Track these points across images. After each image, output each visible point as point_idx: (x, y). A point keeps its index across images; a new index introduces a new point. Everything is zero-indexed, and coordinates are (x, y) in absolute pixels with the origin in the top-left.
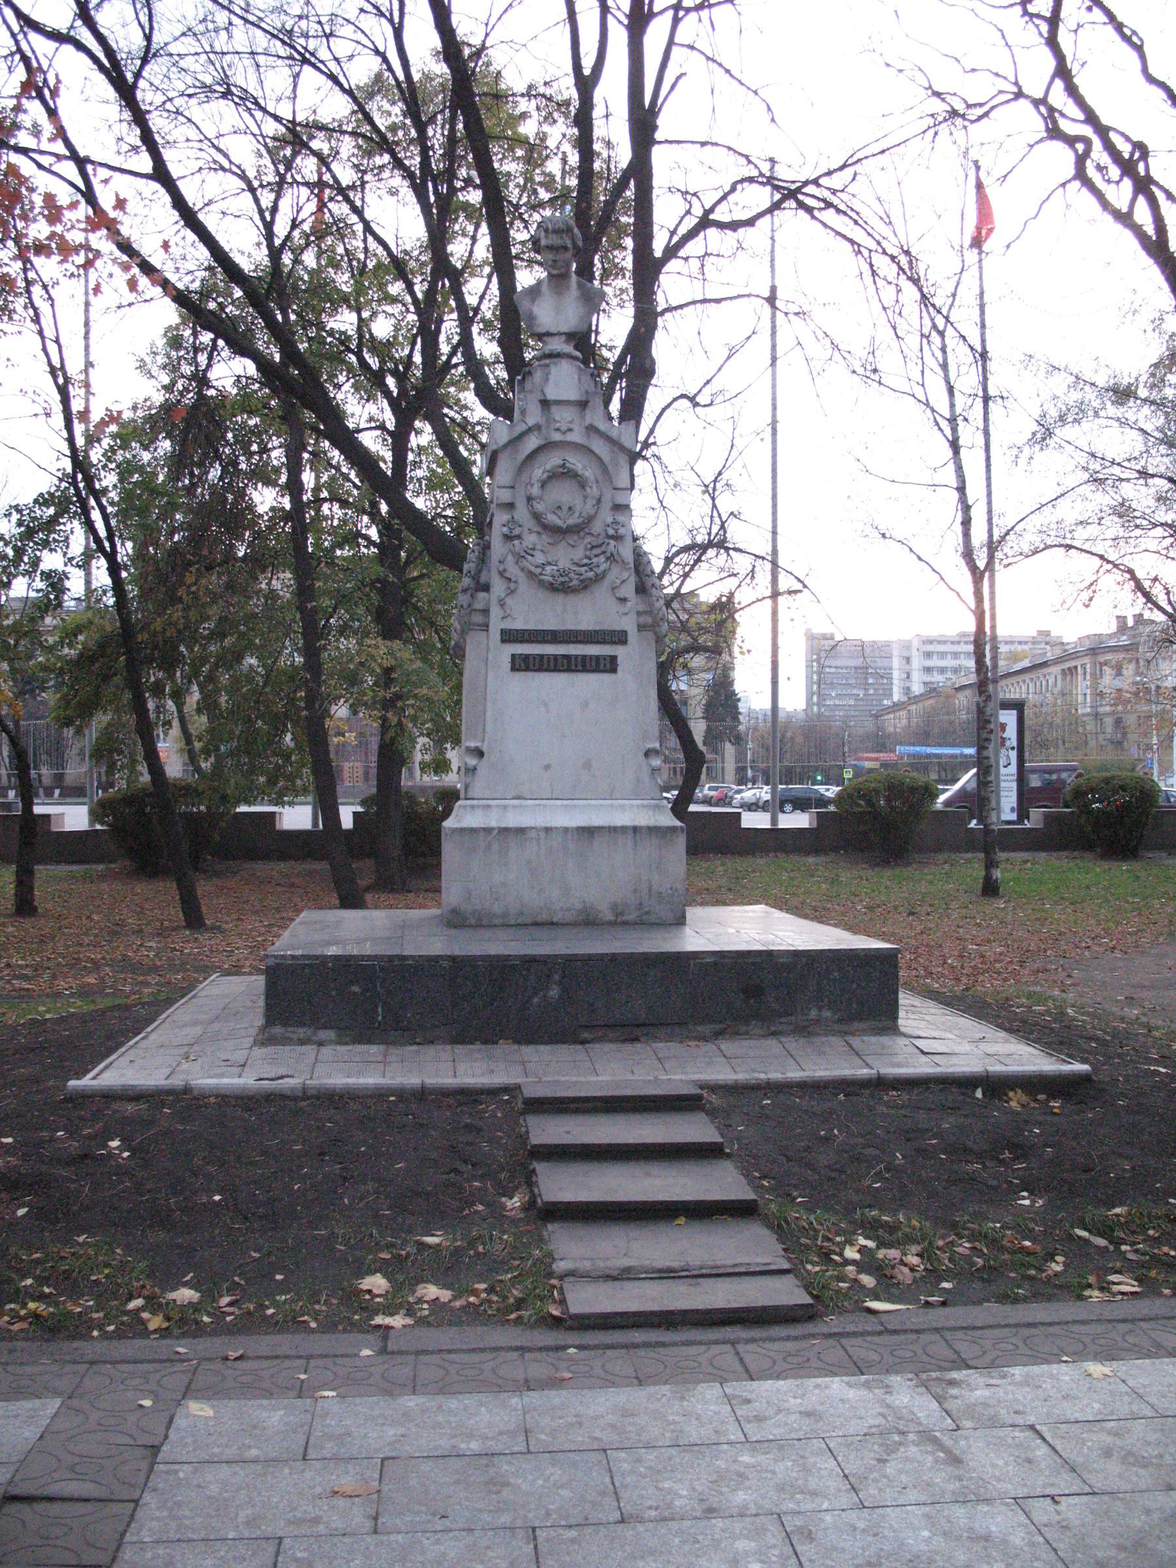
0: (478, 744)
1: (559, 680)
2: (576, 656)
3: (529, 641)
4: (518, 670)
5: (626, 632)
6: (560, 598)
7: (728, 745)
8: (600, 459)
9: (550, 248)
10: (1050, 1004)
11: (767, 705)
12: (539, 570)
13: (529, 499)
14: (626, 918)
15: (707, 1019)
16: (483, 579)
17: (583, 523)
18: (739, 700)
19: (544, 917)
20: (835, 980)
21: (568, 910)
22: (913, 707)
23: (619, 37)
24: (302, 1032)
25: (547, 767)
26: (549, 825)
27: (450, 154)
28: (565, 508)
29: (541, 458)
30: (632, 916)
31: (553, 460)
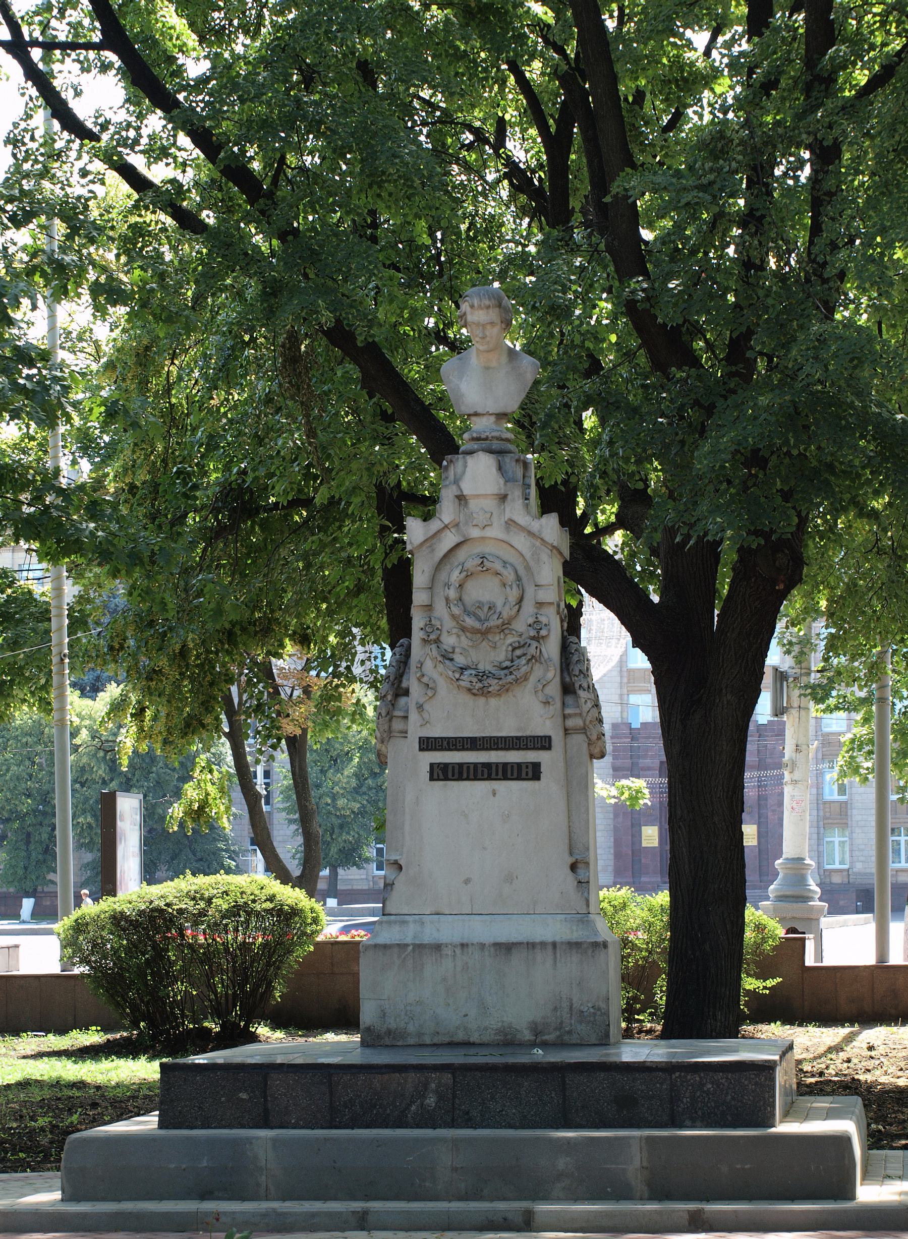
0: (397, 858)
1: (478, 789)
2: (497, 764)
3: (441, 748)
4: (438, 779)
5: (550, 737)
6: (482, 700)
19: (461, 1036)
21: (486, 1029)
25: (467, 881)
28: (486, 609)
30: (550, 1037)
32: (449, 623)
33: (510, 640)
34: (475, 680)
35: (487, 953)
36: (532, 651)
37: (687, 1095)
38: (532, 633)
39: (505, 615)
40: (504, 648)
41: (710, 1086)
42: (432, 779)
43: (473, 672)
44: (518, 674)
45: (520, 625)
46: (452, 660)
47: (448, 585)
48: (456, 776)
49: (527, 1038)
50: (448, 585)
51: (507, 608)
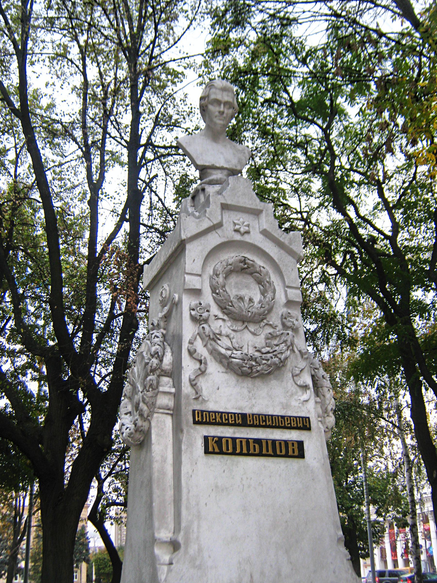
2: (267, 441)
4: (214, 453)
10: (331, 76)
12: (229, 353)
33: (269, 330)
42: (207, 452)
48: (230, 451)
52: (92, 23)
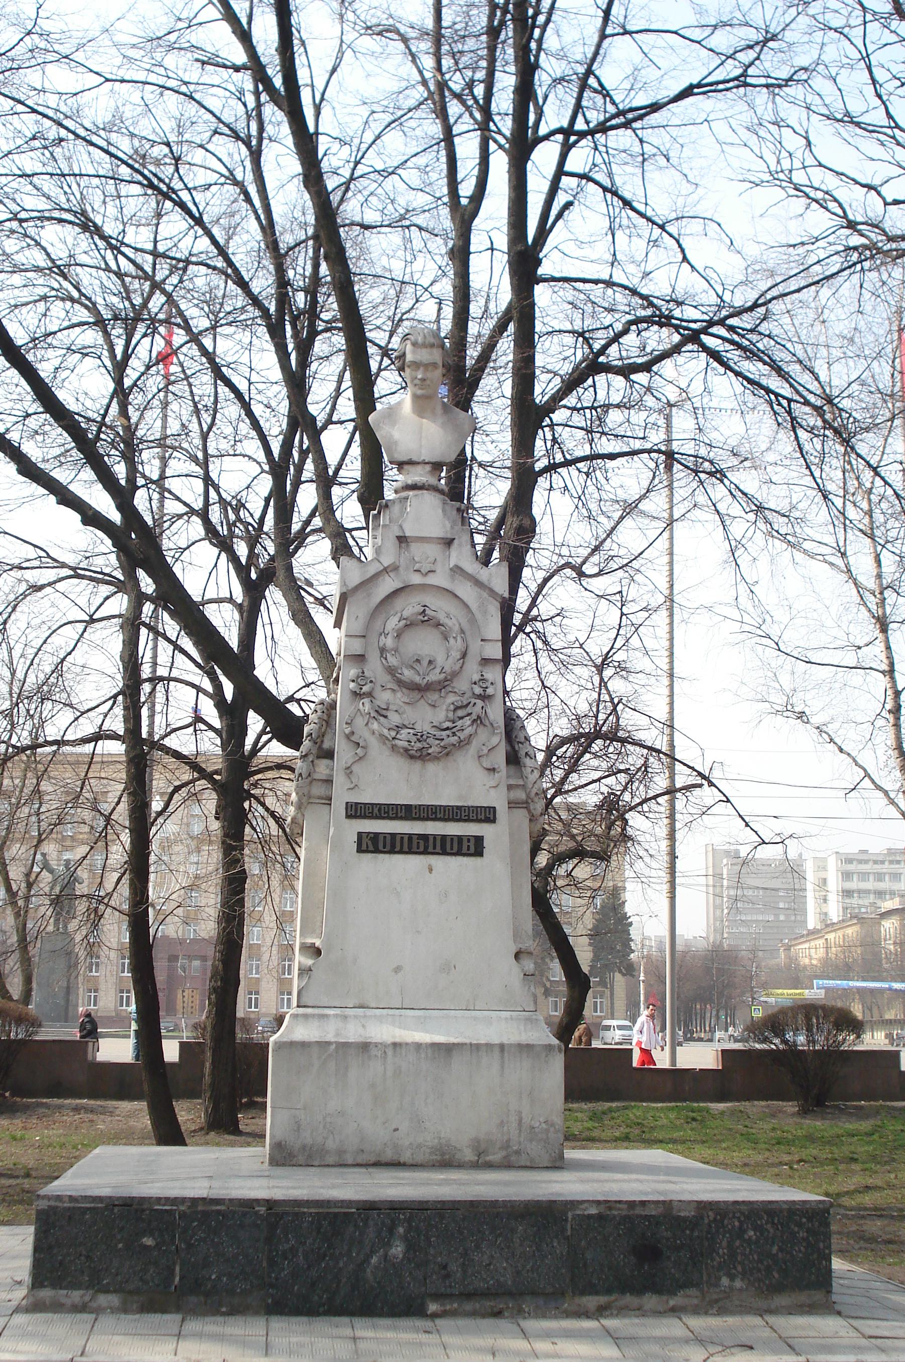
2: (435, 836)
4: (367, 851)
6: (417, 765)
7: (618, 976)
8: (466, 606)
9: (416, 365)
11: (663, 931)
13: (383, 650)
14: (490, 1158)
15: (591, 1290)
16: (326, 745)
17: (446, 680)
18: (631, 924)
19: (389, 1155)
20: (749, 1240)
21: (419, 1146)
22: (831, 936)
23: (500, 162)
24: (76, 1296)
25: (398, 969)
26: (397, 1040)
27: (312, 290)
28: (425, 663)
29: (399, 603)
30: (495, 1157)
31: (409, 607)
32: (383, 678)
33: (451, 698)
34: (414, 739)
35: (423, 1056)
36: (477, 710)
37: (724, 1243)
38: (478, 690)
39: (447, 669)
40: (445, 707)
41: (751, 1233)
42: (360, 850)
43: (411, 731)
44: (463, 735)
45: (462, 684)
46: (386, 717)
47: (384, 633)
48: (388, 848)
49: (467, 1159)
50: (384, 633)
51: (450, 660)
52: (573, 139)
